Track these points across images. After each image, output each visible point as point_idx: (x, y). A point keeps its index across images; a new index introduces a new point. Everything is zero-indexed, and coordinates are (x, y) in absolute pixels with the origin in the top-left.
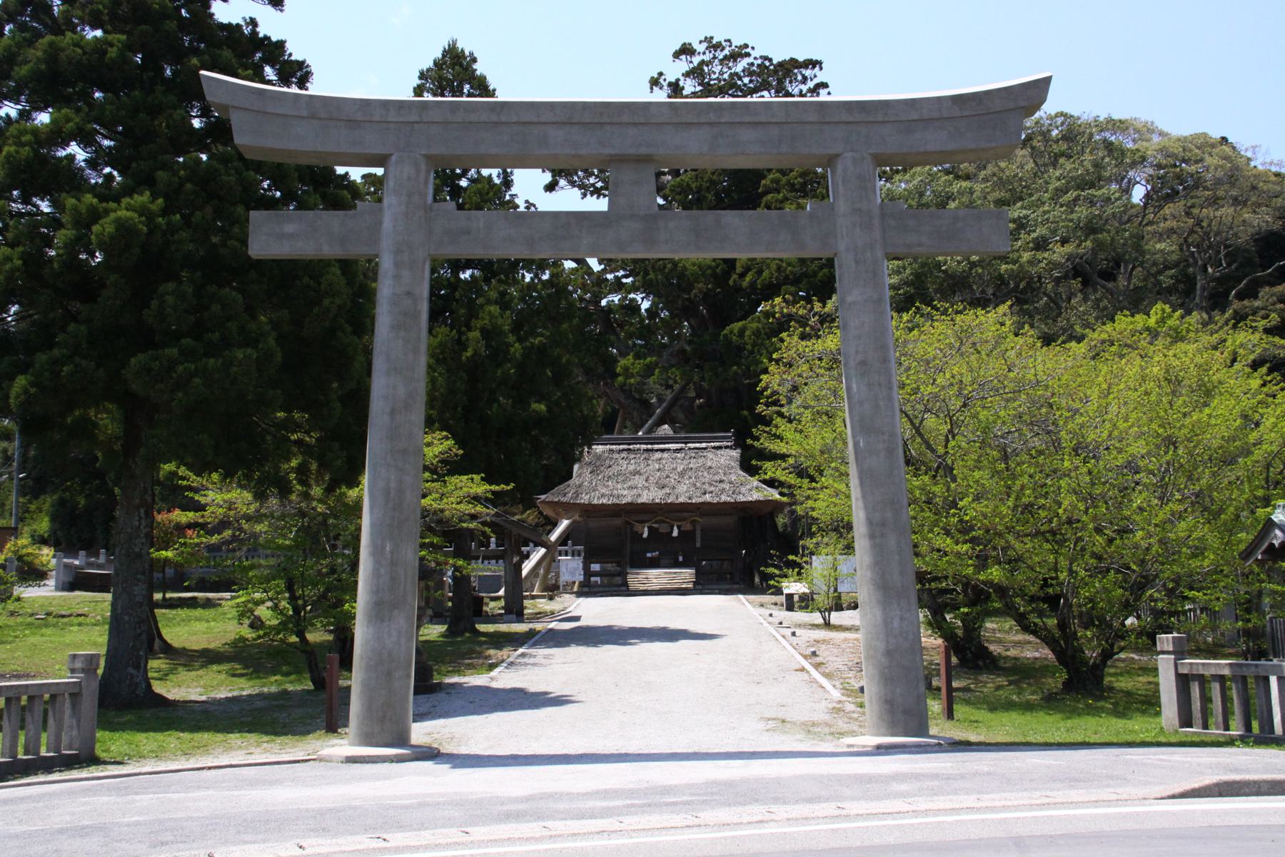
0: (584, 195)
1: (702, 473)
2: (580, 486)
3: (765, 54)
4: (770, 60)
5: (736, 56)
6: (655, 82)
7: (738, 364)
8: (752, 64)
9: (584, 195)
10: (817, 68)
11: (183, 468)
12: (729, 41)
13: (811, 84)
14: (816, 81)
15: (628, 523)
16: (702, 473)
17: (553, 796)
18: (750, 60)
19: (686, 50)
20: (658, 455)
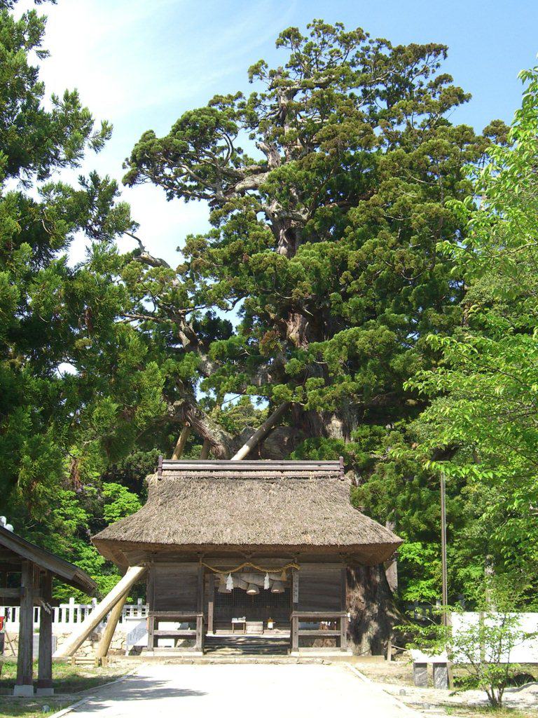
0: (170, 196)
1: (310, 507)
2: (147, 520)
3: (382, 37)
4: (388, 44)
5: (347, 41)
6: (255, 71)
7: (388, 307)
8: (367, 49)
9: (170, 196)
10: (441, 56)
11: (38, 634)
12: (341, 25)
13: (433, 78)
14: (440, 72)
15: (208, 571)
16: (310, 507)
17: (220, 657)
18: (365, 44)
19: (291, 35)
20: (247, 485)
